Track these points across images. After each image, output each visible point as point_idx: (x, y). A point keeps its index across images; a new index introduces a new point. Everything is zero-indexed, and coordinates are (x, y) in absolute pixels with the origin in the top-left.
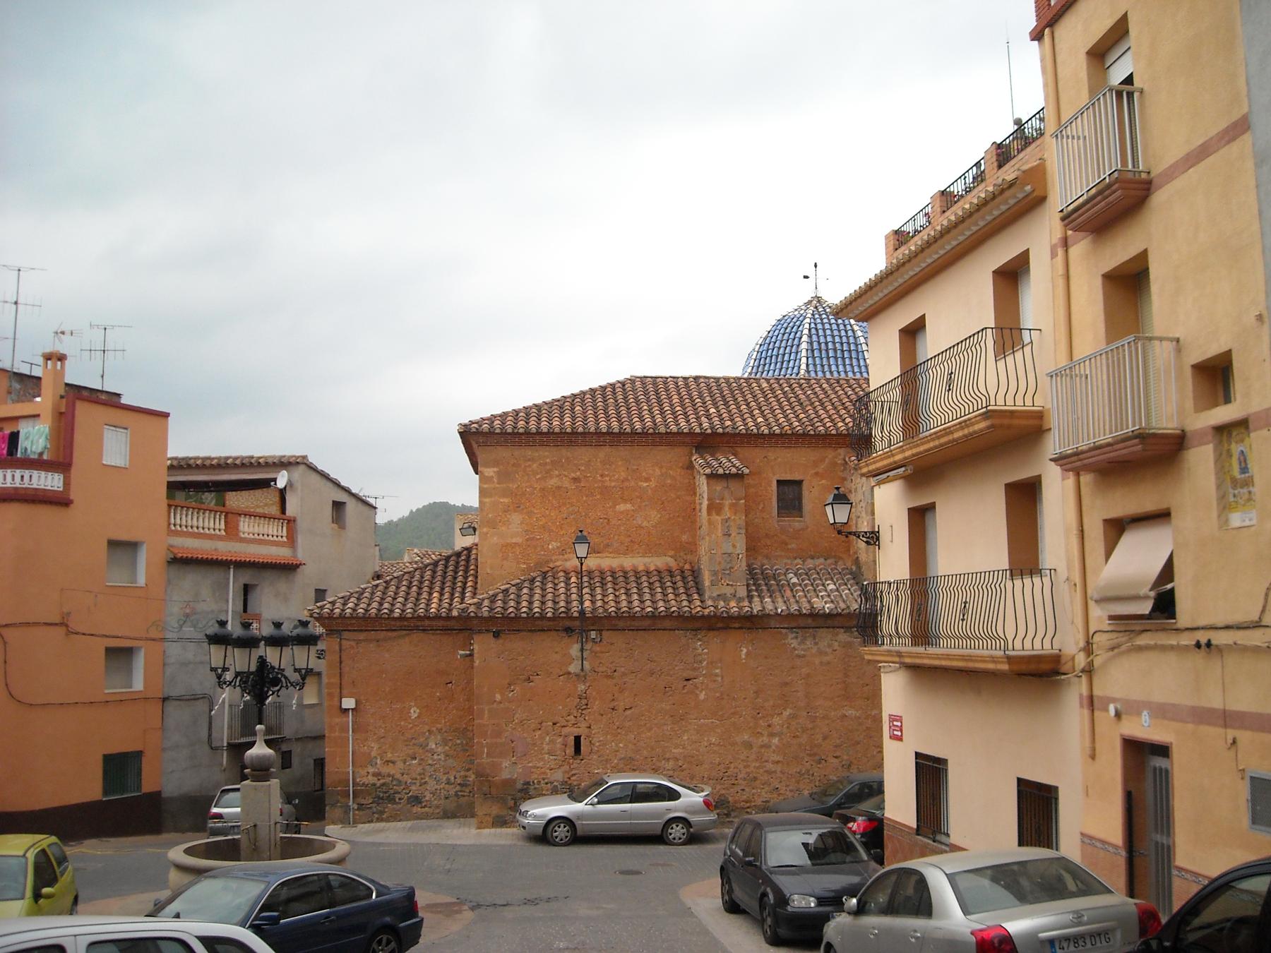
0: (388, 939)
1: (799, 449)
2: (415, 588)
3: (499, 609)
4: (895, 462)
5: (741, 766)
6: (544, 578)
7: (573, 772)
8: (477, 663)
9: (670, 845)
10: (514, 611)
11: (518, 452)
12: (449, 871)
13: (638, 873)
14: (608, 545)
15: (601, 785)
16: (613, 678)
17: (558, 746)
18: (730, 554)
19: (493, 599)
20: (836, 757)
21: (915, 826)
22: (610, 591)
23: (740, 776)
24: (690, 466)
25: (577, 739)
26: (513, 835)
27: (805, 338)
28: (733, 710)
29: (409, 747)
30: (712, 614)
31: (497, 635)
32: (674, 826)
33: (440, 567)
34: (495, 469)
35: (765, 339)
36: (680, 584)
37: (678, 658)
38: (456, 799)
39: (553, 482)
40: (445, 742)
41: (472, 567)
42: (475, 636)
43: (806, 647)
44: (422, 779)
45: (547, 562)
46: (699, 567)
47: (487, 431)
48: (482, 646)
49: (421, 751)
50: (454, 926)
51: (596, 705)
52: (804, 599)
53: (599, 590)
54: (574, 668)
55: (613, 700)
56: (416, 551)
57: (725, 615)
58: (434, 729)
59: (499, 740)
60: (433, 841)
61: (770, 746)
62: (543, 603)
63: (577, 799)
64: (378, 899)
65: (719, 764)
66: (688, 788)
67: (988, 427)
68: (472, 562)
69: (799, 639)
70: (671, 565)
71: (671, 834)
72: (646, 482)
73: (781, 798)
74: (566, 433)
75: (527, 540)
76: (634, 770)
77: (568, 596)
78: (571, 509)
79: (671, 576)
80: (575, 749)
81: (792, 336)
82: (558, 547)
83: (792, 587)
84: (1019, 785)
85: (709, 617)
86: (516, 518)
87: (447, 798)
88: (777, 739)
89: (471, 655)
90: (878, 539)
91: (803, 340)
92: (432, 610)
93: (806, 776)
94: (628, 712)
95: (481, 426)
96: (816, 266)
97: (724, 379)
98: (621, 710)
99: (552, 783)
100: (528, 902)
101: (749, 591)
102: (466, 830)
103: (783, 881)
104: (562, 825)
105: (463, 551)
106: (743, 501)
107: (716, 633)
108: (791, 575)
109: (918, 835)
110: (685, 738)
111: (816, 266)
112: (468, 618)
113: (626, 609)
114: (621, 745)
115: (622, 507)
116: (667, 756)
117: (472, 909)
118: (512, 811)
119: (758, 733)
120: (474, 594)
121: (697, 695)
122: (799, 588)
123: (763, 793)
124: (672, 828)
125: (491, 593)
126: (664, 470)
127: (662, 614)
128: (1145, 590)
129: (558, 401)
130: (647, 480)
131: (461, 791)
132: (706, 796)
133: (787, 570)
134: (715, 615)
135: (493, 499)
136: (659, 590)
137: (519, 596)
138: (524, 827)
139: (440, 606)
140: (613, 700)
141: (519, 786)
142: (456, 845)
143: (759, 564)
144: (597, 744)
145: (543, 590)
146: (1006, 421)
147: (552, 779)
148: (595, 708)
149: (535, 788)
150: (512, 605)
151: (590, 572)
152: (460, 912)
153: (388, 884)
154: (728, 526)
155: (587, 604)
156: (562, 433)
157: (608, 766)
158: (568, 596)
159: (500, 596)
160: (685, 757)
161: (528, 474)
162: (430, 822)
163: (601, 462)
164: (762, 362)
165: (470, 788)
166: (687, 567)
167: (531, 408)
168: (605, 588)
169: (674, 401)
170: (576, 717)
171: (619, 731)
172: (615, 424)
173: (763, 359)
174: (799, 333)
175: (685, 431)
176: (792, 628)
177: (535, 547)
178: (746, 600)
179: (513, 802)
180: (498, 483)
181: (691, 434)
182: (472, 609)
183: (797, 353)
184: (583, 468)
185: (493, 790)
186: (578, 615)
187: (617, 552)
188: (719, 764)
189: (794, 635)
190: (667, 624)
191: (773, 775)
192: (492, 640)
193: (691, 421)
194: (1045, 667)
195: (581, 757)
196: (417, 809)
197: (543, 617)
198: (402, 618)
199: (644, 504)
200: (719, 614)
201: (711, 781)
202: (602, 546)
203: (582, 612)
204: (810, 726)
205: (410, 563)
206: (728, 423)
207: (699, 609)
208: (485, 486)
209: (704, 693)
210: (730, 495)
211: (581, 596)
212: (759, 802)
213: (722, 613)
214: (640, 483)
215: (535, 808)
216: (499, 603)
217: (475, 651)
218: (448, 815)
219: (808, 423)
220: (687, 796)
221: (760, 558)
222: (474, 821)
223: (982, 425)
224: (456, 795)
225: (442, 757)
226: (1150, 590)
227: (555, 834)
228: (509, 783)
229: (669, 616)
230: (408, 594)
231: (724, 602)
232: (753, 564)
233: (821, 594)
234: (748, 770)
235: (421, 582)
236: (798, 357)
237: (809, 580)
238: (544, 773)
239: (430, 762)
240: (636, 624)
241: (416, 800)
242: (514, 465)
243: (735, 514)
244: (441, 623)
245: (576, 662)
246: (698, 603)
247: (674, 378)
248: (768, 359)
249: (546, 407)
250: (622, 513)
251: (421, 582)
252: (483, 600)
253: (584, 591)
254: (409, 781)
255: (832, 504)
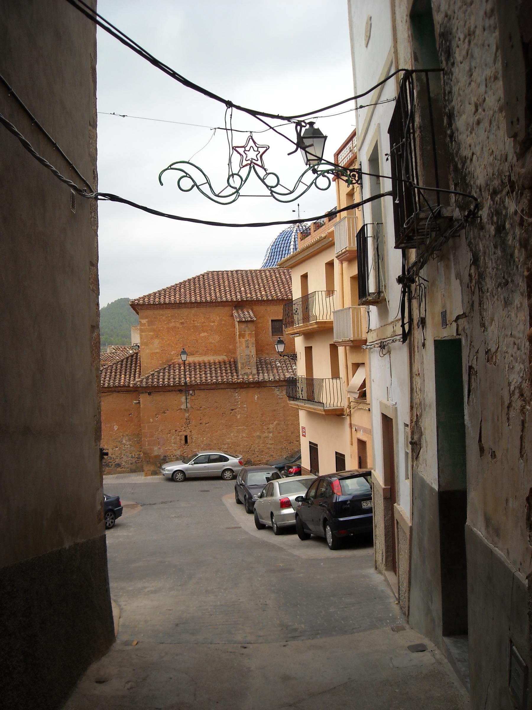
0: (111, 514)
1: (281, 305)
2: (113, 373)
3: (150, 383)
4: (295, 332)
5: (256, 446)
6: (170, 367)
7: (185, 451)
8: (142, 406)
9: (225, 480)
10: (157, 383)
11: (156, 312)
12: (133, 493)
13: (208, 491)
14: (197, 352)
15: (196, 456)
16: (201, 410)
17: (178, 440)
18: (249, 355)
19: (147, 378)
20: (297, 441)
21: (310, 470)
22: (198, 372)
23: (256, 450)
24: (232, 316)
25: (186, 437)
26: (160, 478)
27: (292, 243)
28: (252, 422)
29: (114, 443)
30: (241, 382)
31: (150, 394)
32: (227, 472)
33: (124, 363)
34: (147, 320)
35: (274, 243)
36: (228, 368)
37: (228, 401)
38: (135, 464)
39: (172, 324)
40: (130, 440)
41: (138, 362)
42: (140, 395)
43: (283, 394)
44: (120, 456)
45: (171, 360)
46: (237, 360)
47: (142, 304)
48: (144, 399)
49: (119, 444)
50: (135, 512)
51: (193, 422)
52: (282, 374)
53: (193, 373)
54: (183, 407)
55: (201, 420)
56: (113, 346)
57: (247, 382)
58: (125, 434)
59: (153, 439)
60: (127, 482)
61: (269, 437)
62: (169, 379)
63: (185, 462)
64: (107, 500)
65: (247, 445)
66: (233, 456)
67: (318, 327)
68: (139, 359)
69: (280, 391)
70: (225, 359)
71: (225, 476)
72: (213, 323)
73: (274, 459)
74: (177, 303)
75: (162, 351)
76: (210, 449)
77: (180, 375)
78: (180, 336)
79: (225, 365)
80: (185, 441)
81: (286, 242)
82: (175, 353)
83: (277, 368)
84: (336, 454)
85: (240, 383)
86: (156, 341)
87: (131, 464)
88: (272, 434)
89: (139, 403)
90: (296, 357)
91: (291, 244)
92: (122, 383)
93: (284, 450)
94: (207, 425)
95: (139, 301)
96: (298, 205)
97: (250, 271)
98: (204, 424)
99: (176, 456)
100: (162, 503)
101: (258, 370)
102: (140, 477)
103: (252, 491)
104: (180, 473)
105: (134, 355)
106: (254, 332)
107: (244, 389)
108: (278, 362)
109: (311, 473)
110: (232, 435)
111: (298, 205)
112: (137, 387)
113: (204, 381)
114: (205, 439)
115: (203, 335)
116: (225, 443)
117: (142, 506)
118: (159, 468)
119: (263, 432)
120: (139, 377)
121: (236, 416)
122: (280, 368)
123: (266, 457)
124: (226, 473)
125: (147, 376)
126: (221, 317)
127: (220, 382)
128: (356, 391)
129: (174, 286)
130: (214, 322)
131: (138, 461)
132: (240, 459)
133: (276, 360)
134: (243, 382)
135: (146, 333)
136: (219, 371)
137: (159, 376)
138: (164, 475)
139: (125, 381)
140: (201, 420)
141: (162, 457)
142: (136, 483)
143: (264, 357)
144: (194, 439)
145: (169, 373)
146: (323, 325)
147: (176, 454)
148: (193, 423)
149: (169, 458)
150: (156, 381)
151: (189, 364)
152: (136, 507)
153: (111, 496)
154: (248, 343)
155: (188, 379)
156: (175, 303)
157: (199, 448)
158: (180, 375)
159: (151, 377)
160: (232, 443)
161: (161, 322)
162: (125, 474)
163: (193, 315)
164: (273, 254)
165: (141, 459)
166: (232, 360)
167: (161, 291)
168: (196, 371)
169: (226, 284)
170: (185, 427)
171: (204, 433)
172: (198, 298)
173: (273, 253)
174: (290, 240)
175: (229, 300)
176: (277, 386)
177: (165, 354)
178: (257, 375)
179: (159, 464)
180: (148, 326)
181: (232, 301)
182: (138, 383)
183: (289, 250)
184: (185, 318)
185: (151, 460)
186: (184, 384)
187: (201, 354)
188: (247, 445)
189: (278, 389)
190: (222, 386)
191: (270, 449)
192: (148, 396)
193: (232, 295)
194: (338, 413)
195: (188, 444)
196: (119, 469)
197: (169, 386)
198: (109, 387)
199: (212, 333)
200: (244, 382)
201: (243, 453)
202: (195, 352)
203: (186, 383)
204: (286, 428)
205: (110, 353)
206: (249, 295)
207: (236, 380)
208: (142, 328)
209: (239, 415)
210: (249, 330)
211: (185, 375)
212: (264, 461)
213: (246, 381)
214: (210, 324)
215: (168, 467)
216: (150, 380)
217: (141, 401)
218: (133, 471)
219: (284, 294)
220: (232, 459)
221: (264, 355)
222: (143, 473)
223: (315, 326)
224: (136, 462)
225: (129, 446)
226: (358, 391)
227: (177, 477)
228: (157, 457)
229: (223, 383)
230: (111, 376)
231: (247, 376)
232: (261, 357)
233: (289, 371)
234: (259, 448)
235: (116, 370)
236: (289, 252)
237: (285, 364)
238: (172, 452)
239: (124, 449)
240: (209, 387)
241: (118, 465)
242: (155, 318)
243: (251, 338)
244: (125, 389)
245: (184, 404)
246: (236, 377)
247: (227, 271)
248: (275, 253)
249: (168, 290)
250: (203, 337)
251: (116, 370)
252: (143, 379)
253: (187, 373)
254: (115, 457)
255: (277, 344)
